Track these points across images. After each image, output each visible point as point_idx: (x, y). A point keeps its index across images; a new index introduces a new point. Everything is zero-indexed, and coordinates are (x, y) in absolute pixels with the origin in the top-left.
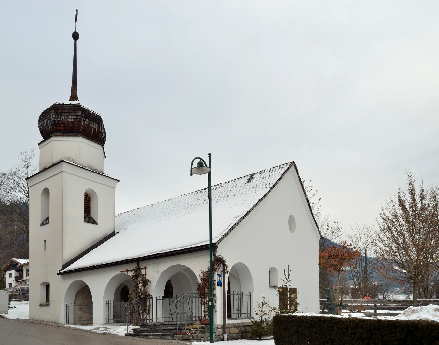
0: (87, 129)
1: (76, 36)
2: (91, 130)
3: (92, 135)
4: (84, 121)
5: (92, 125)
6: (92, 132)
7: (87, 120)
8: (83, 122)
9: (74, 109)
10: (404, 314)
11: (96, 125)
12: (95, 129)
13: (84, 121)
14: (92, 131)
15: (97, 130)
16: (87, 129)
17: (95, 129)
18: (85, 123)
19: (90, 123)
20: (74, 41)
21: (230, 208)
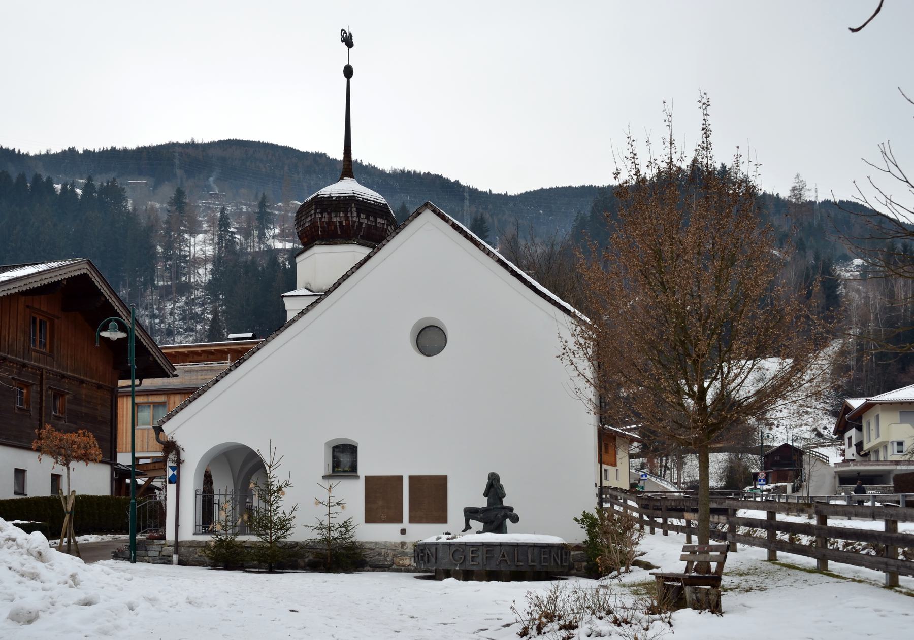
0: (328, 228)
1: (348, 72)
2: (336, 227)
3: (339, 233)
4: (321, 218)
5: (334, 219)
6: (339, 229)
7: (326, 214)
8: (319, 220)
9: (304, 217)
10: (33, 573)
11: (342, 214)
12: (341, 222)
13: (321, 218)
14: (337, 228)
15: (344, 222)
16: (328, 228)
17: (341, 222)
18: (323, 220)
19: (330, 218)
20: (346, 79)
21: (355, 638)
